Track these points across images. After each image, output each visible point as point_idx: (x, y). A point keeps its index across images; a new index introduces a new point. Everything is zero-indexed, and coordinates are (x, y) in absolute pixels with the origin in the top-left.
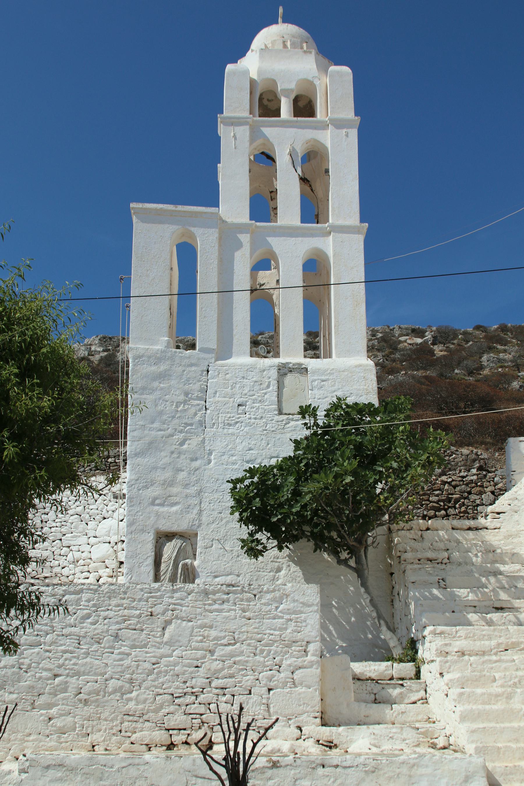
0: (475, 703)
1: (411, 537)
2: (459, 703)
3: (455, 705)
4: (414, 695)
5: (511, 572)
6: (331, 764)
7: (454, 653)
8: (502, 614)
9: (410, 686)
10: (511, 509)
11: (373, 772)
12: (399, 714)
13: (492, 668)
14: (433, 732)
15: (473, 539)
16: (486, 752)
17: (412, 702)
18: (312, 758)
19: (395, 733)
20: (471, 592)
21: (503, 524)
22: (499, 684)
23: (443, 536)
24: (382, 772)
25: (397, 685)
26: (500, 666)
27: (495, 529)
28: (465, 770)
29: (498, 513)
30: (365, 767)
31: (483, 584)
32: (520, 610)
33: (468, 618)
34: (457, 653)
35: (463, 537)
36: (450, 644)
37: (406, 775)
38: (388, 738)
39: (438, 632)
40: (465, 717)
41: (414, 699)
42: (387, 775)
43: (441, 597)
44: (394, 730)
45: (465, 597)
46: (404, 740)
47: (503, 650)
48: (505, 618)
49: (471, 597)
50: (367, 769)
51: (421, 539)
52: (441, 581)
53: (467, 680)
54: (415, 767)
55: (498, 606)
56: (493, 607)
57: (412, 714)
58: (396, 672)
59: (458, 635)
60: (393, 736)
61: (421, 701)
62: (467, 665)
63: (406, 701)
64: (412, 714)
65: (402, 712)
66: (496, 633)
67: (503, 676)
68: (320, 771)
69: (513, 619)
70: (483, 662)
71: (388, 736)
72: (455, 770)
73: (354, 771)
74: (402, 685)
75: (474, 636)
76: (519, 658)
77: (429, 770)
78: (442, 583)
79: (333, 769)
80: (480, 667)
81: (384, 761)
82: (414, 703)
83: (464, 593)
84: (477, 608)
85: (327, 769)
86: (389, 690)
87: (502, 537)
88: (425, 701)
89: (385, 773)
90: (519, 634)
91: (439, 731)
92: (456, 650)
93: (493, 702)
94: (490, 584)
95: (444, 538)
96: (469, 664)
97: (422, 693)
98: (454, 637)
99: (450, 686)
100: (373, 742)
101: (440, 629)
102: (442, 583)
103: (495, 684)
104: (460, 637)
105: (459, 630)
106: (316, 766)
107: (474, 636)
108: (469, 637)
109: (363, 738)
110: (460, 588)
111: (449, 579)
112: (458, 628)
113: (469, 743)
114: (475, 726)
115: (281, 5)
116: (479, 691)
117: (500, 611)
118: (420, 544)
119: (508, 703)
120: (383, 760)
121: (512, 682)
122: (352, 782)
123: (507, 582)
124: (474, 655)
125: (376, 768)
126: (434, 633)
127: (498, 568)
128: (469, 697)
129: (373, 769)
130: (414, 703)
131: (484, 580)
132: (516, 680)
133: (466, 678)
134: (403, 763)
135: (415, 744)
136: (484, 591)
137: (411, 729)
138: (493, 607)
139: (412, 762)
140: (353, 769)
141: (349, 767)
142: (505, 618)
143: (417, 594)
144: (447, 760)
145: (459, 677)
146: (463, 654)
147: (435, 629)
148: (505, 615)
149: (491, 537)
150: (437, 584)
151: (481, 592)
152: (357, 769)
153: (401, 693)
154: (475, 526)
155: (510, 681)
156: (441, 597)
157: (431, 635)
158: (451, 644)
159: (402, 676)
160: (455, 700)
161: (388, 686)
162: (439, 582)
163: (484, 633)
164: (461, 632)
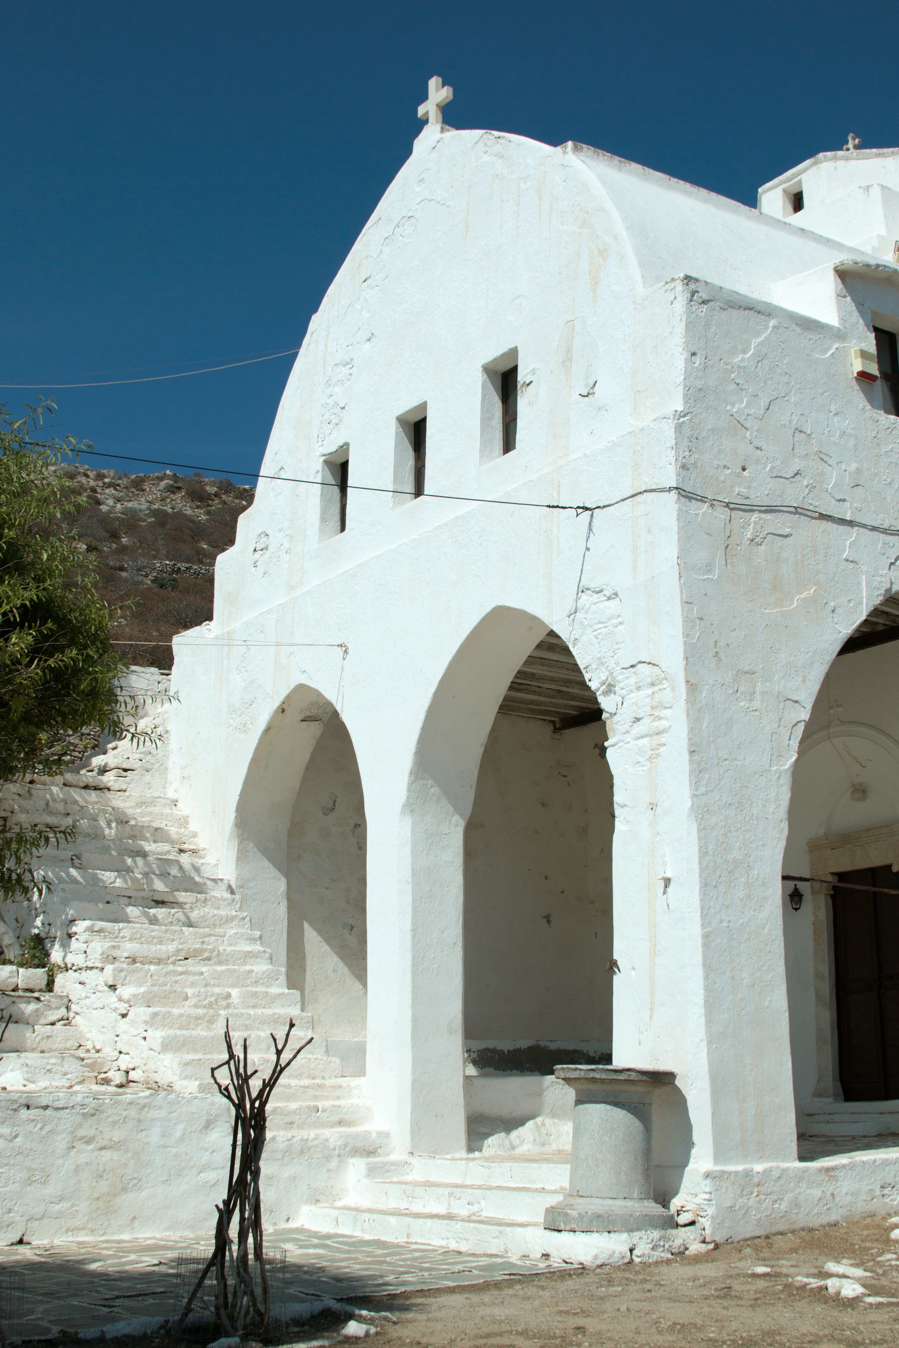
0: (171, 1027)
1: (15, 791)
2: (151, 1026)
3: (145, 1028)
4: (52, 1014)
5: (158, 854)
6: (39, 1105)
7: (123, 959)
8: (169, 910)
9: (49, 1001)
10: (141, 767)
11: (93, 1115)
12: (43, 1039)
13: (176, 982)
14: (102, 1064)
15: (96, 803)
16: (211, 1090)
17: (49, 1022)
18: (15, 1096)
19: (55, 1064)
20: (119, 876)
21: (130, 786)
22: (192, 1004)
23: (58, 794)
24: (104, 1115)
25: (32, 999)
26: (187, 980)
27: (119, 791)
28: (207, 1113)
29: (125, 770)
30: (83, 1109)
31: (129, 867)
32: (185, 906)
33: (126, 913)
34: (127, 960)
35: (83, 798)
36: (118, 947)
37: (134, 1119)
38: (45, 1071)
39: (96, 929)
40: (167, 1045)
41: (52, 1018)
42: (110, 1119)
43: (81, 880)
44: (53, 1061)
45: (112, 883)
46: (65, 1074)
47: (183, 958)
48: (173, 915)
49: (119, 883)
50: (85, 1111)
51: (28, 796)
52: (74, 857)
53: (154, 997)
54: (146, 1109)
55: (159, 899)
56: (153, 900)
57: (59, 1039)
58: (23, 980)
59: (121, 935)
60: (52, 1069)
61: (62, 1022)
62: (147, 976)
63: (42, 1021)
64: (59, 1039)
65: (48, 1036)
66: (168, 935)
67: (197, 994)
68: (24, 1114)
69: (183, 918)
70: (167, 973)
71: (44, 1068)
72: (195, 1113)
73: (68, 1114)
74: (38, 999)
75: (141, 938)
76: (209, 971)
77: (162, 1113)
78: (76, 861)
79: (41, 1111)
80: (162, 980)
81: (107, 1101)
82: (53, 1024)
83: (110, 878)
84: (133, 899)
85: (33, 1112)
86: (21, 1006)
87: (133, 804)
88: (67, 1021)
89: (109, 1117)
90: (195, 939)
91: (110, 1063)
92: (126, 955)
93: (192, 1026)
94: (137, 867)
95: (58, 797)
96: (149, 974)
97: (62, 1012)
98: (117, 937)
99: (132, 1004)
100: (26, 1076)
101: (100, 924)
102: (76, 861)
103: (187, 1003)
104: (123, 937)
105: (123, 929)
106: (18, 1107)
107: (141, 938)
108: (135, 939)
109: (12, 1071)
110: (105, 870)
111: (86, 856)
112: (121, 925)
113: (181, 1079)
114: (190, 1057)
115: (439, 75)
116: (176, 1011)
117: (160, 905)
118: (27, 801)
119: (209, 1029)
120: (106, 1099)
121: (207, 1002)
122: (66, 1129)
123: (158, 866)
124: (148, 963)
125: (97, 1110)
126: (91, 930)
127: (141, 846)
128: (164, 1019)
129: (94, 1112)
130: (53, 1024)
131: (129, 861)
132: (213, 999)
133: (153, 994)
134: (132, 1103)
135: (78, 1080)
136: (136, 877)
137: (74, 1060)
138: (153, 900)
139: (142, 1102)
140: (67, 1111)
141: (63, 1108)
142: (173, 915)
143: (50, 873)
144: (185, 1100)
145: (144, 992)
146: (134, 961)
147: (93, 925)
148: (173, 911)
149: (117, 801)
150: (70, 861)
151: (131, 878)
152: (73, 1111)
153: (37, 1010)
154: (94, 785)
155: (205, 999)
156: (81, 880)
157: (86, 933)
158: (119, 946)
159: (31, 986)
160: (146, 1022)
161: (20, 999)
162: (72, 860)
163: (153, 934)
164: (124, 931)
